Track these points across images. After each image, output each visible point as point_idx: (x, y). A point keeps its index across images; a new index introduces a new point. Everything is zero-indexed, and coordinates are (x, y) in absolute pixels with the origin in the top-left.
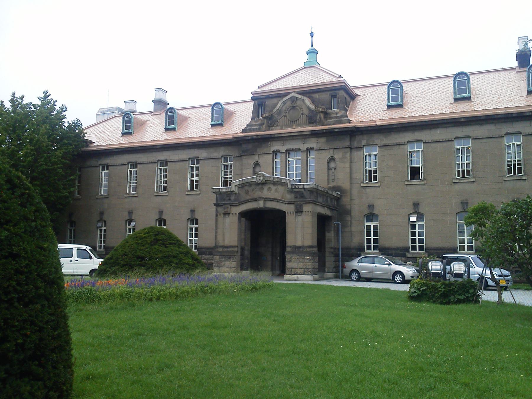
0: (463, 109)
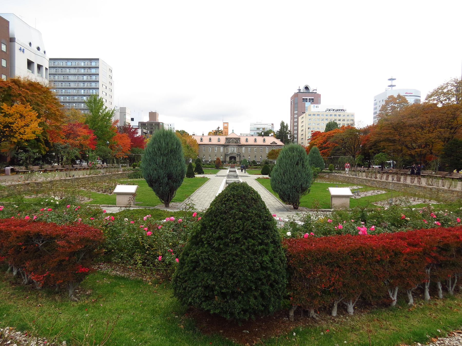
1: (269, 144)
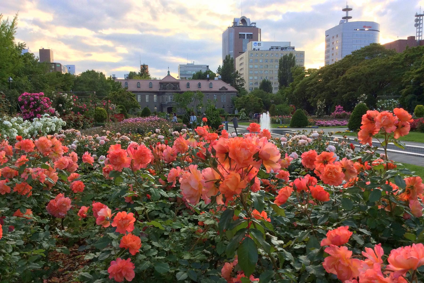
1: (218, 90)
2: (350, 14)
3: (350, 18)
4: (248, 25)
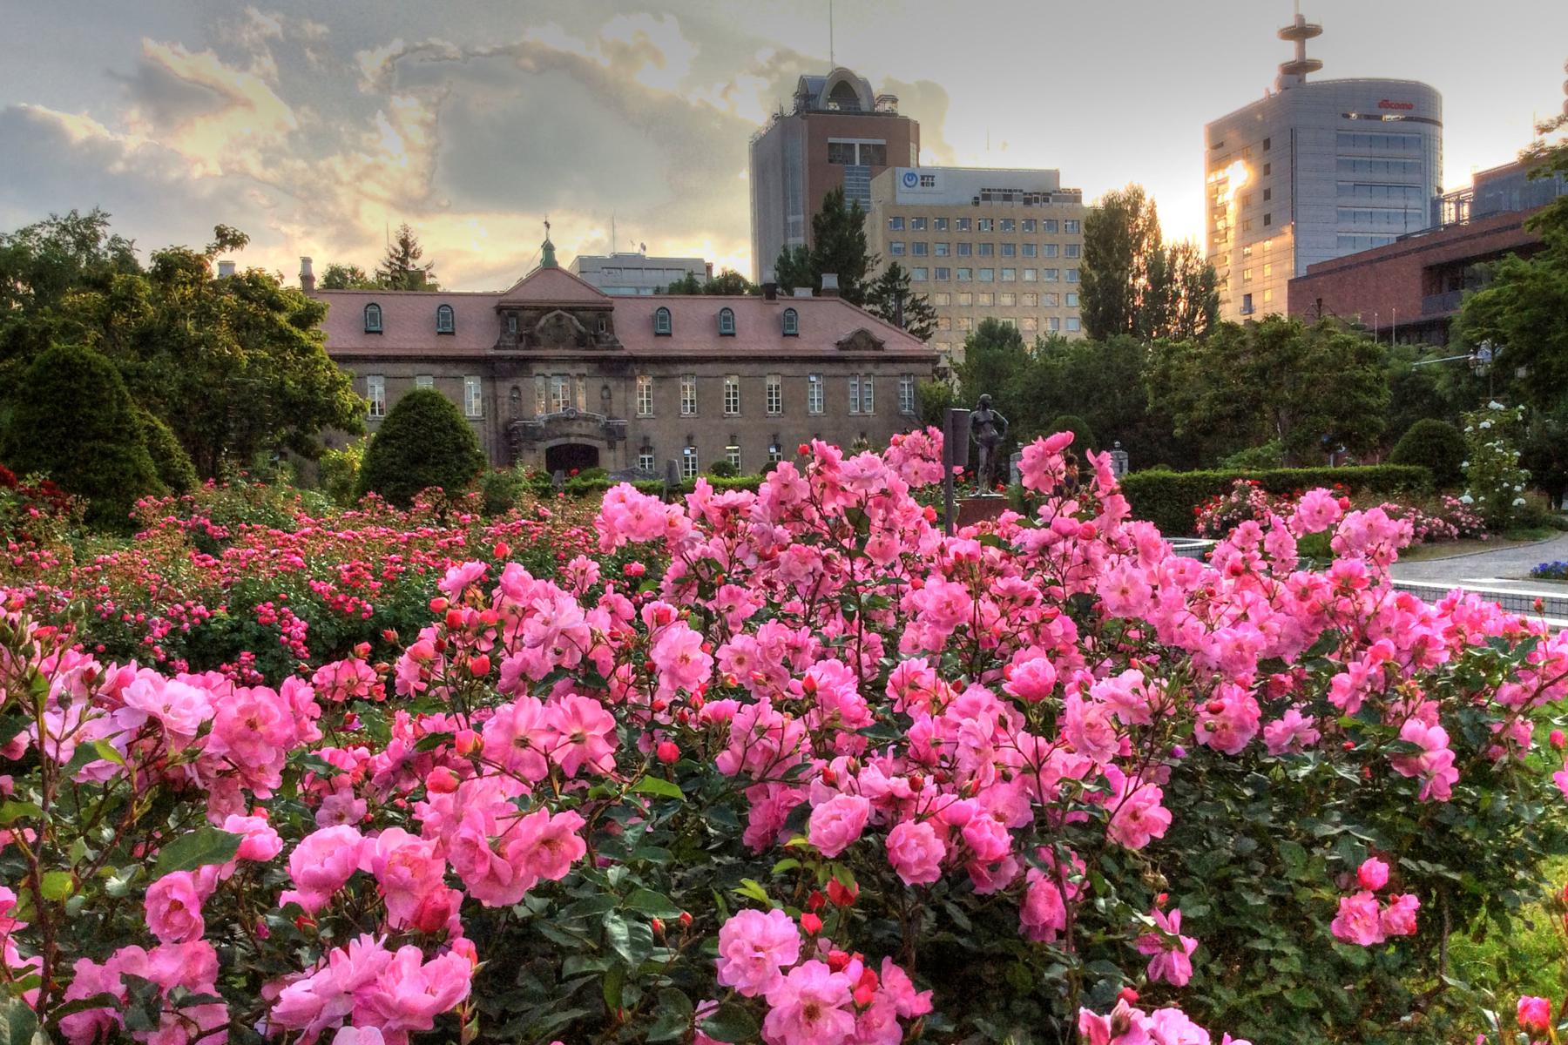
0: (371, 346)
1: (829, 349)
2: (1313, 49)
3: (1315, 66)
4: (864, 105)
